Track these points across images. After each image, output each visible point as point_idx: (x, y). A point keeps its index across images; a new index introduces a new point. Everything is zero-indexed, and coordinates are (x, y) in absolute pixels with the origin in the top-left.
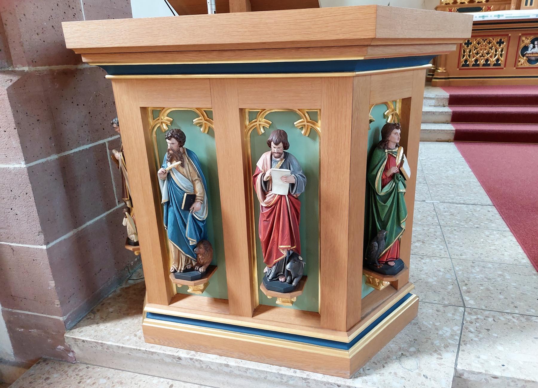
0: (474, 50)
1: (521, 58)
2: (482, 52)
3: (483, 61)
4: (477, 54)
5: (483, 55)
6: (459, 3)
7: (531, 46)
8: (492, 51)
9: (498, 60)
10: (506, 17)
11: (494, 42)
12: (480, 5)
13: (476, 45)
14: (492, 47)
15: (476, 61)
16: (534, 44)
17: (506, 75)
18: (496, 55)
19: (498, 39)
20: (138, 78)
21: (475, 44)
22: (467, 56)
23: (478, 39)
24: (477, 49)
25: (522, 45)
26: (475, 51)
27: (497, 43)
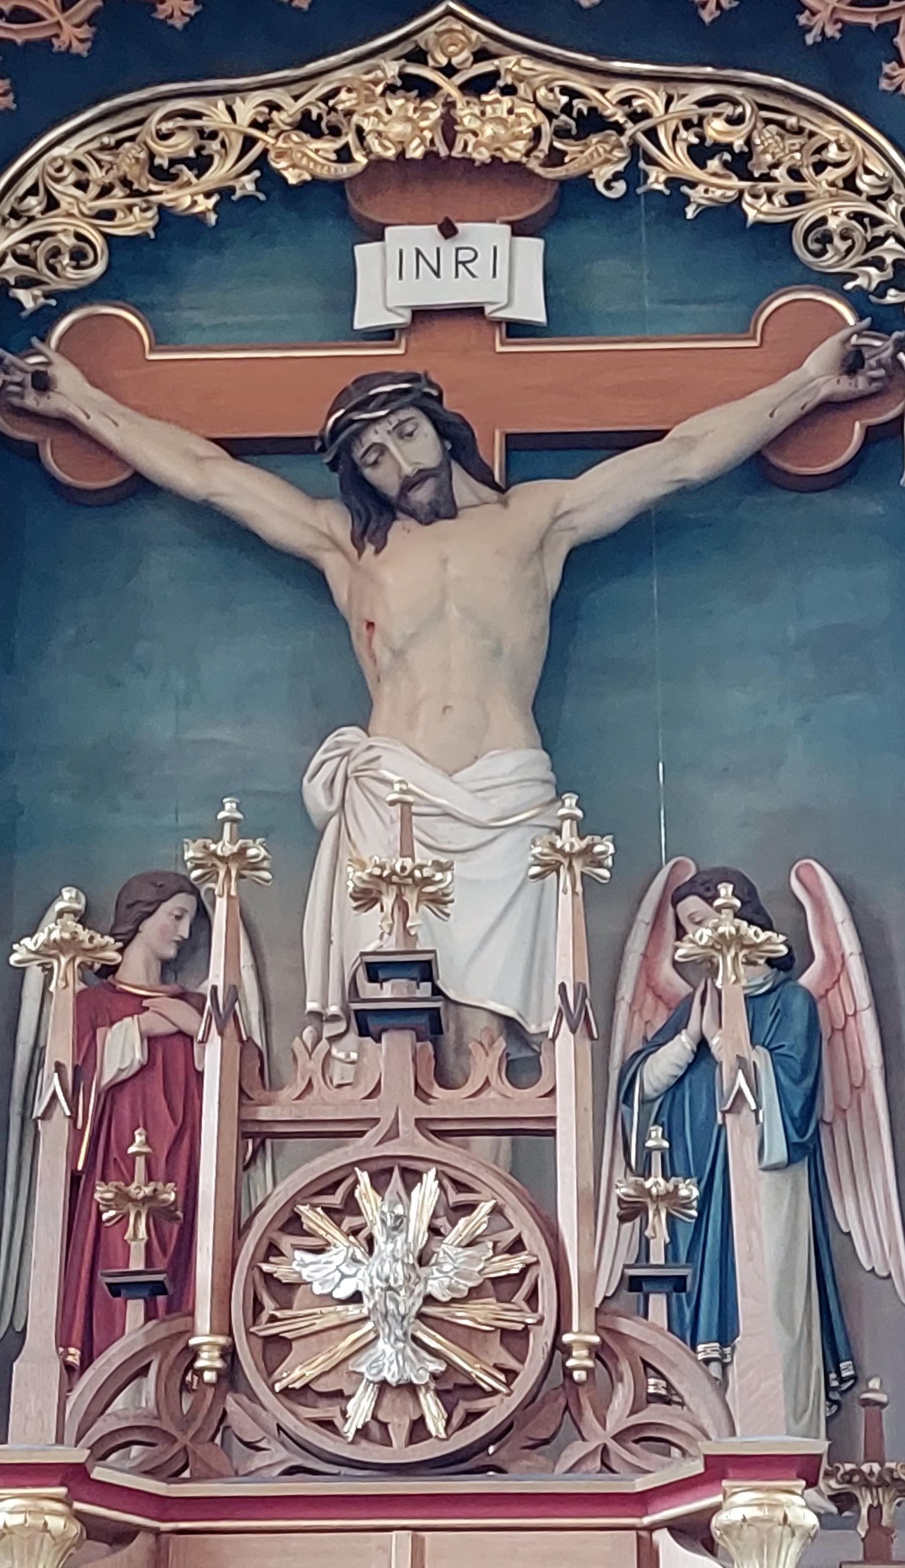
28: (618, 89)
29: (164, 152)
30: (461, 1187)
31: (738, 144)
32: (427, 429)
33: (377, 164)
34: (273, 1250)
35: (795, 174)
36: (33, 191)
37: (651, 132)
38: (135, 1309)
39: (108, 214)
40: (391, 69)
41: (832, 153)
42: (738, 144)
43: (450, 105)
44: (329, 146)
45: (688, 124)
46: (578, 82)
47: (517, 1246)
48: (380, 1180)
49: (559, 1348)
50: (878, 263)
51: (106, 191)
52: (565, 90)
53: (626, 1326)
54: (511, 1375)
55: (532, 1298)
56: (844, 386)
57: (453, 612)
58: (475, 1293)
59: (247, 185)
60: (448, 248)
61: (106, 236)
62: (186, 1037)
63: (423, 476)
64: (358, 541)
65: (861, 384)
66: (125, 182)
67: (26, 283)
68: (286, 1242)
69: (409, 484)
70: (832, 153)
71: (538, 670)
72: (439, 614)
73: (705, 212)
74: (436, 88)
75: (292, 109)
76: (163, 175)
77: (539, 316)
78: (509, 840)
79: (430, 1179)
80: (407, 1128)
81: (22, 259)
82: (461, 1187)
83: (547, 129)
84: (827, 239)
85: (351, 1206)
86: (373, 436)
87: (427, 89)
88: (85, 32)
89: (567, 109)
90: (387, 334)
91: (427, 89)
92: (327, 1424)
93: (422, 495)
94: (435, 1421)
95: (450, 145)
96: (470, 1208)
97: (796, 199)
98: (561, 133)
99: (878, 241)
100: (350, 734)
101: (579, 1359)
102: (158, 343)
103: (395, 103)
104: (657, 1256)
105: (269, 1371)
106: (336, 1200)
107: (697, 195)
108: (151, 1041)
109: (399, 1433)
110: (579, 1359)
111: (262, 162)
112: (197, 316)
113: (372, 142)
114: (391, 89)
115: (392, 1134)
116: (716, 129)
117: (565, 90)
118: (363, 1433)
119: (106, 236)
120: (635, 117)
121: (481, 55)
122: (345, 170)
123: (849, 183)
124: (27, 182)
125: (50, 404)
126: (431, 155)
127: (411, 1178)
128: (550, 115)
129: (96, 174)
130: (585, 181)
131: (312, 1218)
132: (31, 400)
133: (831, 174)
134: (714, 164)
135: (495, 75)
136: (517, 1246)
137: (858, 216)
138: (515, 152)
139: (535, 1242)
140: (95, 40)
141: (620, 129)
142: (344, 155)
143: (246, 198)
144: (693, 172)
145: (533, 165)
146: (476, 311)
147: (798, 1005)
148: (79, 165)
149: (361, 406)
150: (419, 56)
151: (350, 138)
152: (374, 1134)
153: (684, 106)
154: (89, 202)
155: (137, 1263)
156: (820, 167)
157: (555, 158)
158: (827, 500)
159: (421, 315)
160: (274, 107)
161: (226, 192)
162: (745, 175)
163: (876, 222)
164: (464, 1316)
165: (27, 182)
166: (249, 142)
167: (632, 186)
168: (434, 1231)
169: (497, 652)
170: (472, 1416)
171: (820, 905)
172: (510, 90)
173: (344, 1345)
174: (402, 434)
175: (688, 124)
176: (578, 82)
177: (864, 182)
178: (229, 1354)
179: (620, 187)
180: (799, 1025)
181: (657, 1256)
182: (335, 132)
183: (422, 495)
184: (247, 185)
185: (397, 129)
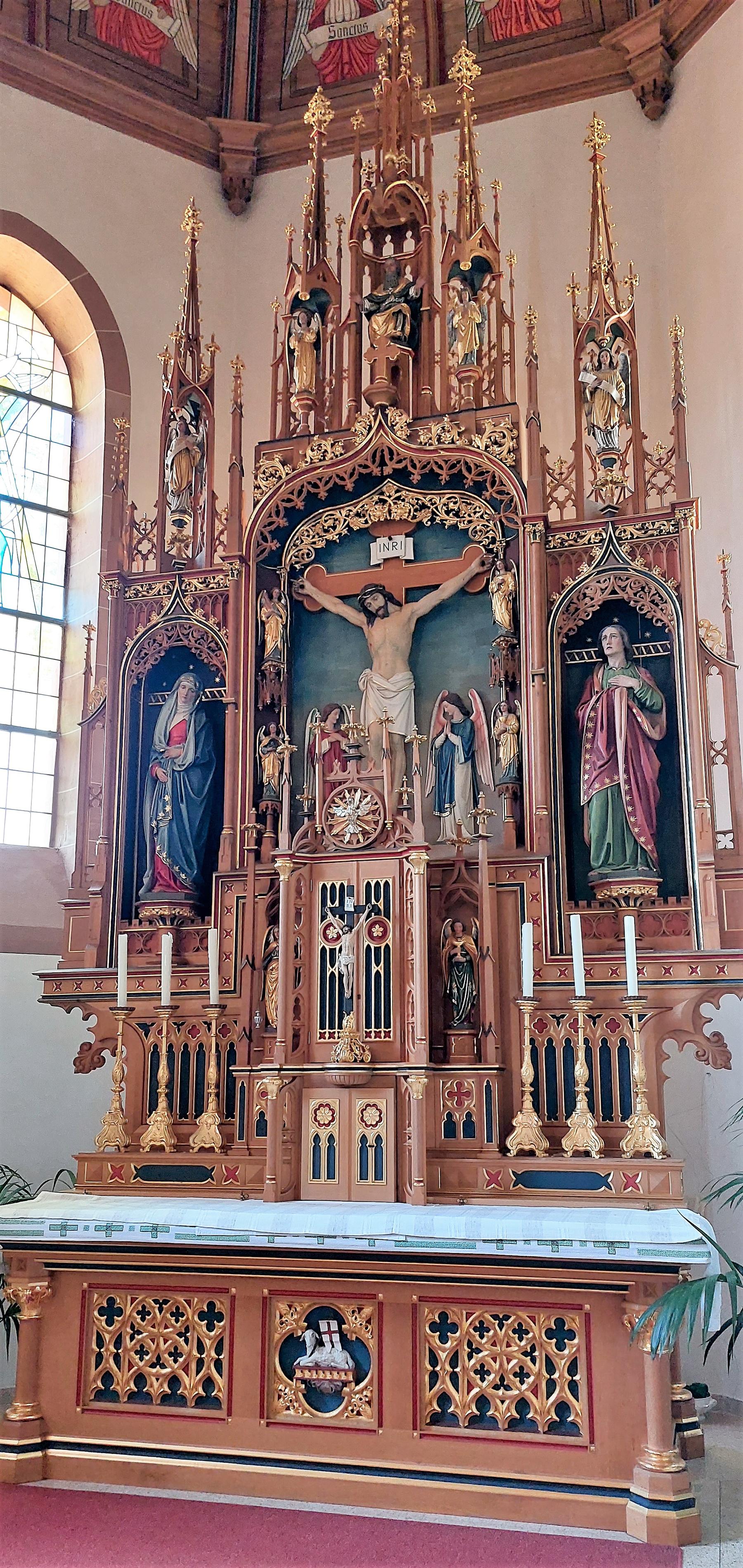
0: (470, 1357)
1: (281, 1381)
2: (496, 1366)
3: (508, 1409)
4: (482, 1372)
5: (502, 1379)
6: (513, 1152)
7: (309, 1336)
8: (535, 1369)
9: (562, 1408)
10: (178, 1236)
11: (537, 1331)
12: (205, 1161)
13: (135, 1319)
14: (533, 1349)
15: (482, 1402)
16: (317, 1329)
17: (385, 1459)
18: (551, 1385)
19: (549, 1318)
20: (259, 1471)
21: (468, 1333)
22: (562, 1390)
23: (140, 1298)
24: (478, 1351)
25: (278, 1336)
26: (473, 1361)
27: (550, 1333)
28: (428, 497)
29: (326, 525)
30: (365, 792)
31: (456, 508)
32: (381, 597)
33: (374, 523)
34: (330, 807)
35: (469, 515)
36: (297, 539)
37: (436, 508)
38: (306, 819)
39: (314, 543)
40: (376, 498)
41: (478, 509)
42: (456, 508)
43: (390, 505)
44: (362, 520)
45: (445, 505)
46: (420, 497)
47: (376, 804)
48: (349, 792)
49: (385, 824)
50: (488, 538)
51: (314, 537)
52: (416, 499)
53: (399, 818)
54: (375, 829)
55: (379, 814)
56: (481, 569)
57: (387, 641)
58: (368, 814)
59: (345, 532)
60: (391, 542)
61: (315, 549)
62: (339, 742)
63: (380, 608)
64: (368, 624)
65: (485, 568)
66: (318, 534)
67: (297, 563)
68: (332, 805)
69: (378, 610)
70: (478, 509)
71: (409, 650)
72: (384, 641)
73: (449, 527)
74: (386, 501)
75: (355, 511)
76: (326, 531)
77: (411, 557)
78: (401, 694)
79: (359, 791)
80: (356, 780)
81: (296, 557)
82: (365, 792)
83: (412, 510)
84: (476, 532)
85: (344, 797)
86: (368, 601)
87: (384, 502)
88: (303, 503)
89: (417, 503)
90: (378, 565)
91: (384, 502)
92: (342, 841)
93: (380, 613)
94: (361, 840)
95: (390, 516)
96: (366, 796)
97: (470, 522)
98: (416, 510)
99: (488, 532)
100: (368, 671)
101: (389, 826)
102: (328, 573)
103: (377, 507)
104: (405, 803)
105: (330, 831)
106: (341, 796)
107: (447, 523)
108: (331, 743)
109: (355, 842)
110: (389, 826)
111: (348, 525)
112: (338, 564)
113: (372, 518)
114: (376, 503)
115: (353, 781)
116: (451, 505)
117: (416, 499)
118: (348, 842)
119: (315, 549)
120: (432, 504)
121: (397, 492)
122: (366, 526)
123: (482, 517)
124: (296, 537)
125: (305, 592)
126: (386, 519)
127: (356, 791)
128: (413, 506)
129: (311, 533)
130: (421, 522)
131: (337, 800)
132: (300, 591)
133: (478, 515)
134: (451, 514)
135: (400, 496)
136: (376, 804)
137: (483, 525)
138: (405, 516)
139: (379, 803)
140: (305, 505)
141: (429, 508)
142: (366, 522)
143: (346, 535)
144: (446, 517)
145: (409, 519)
146: (398, 557)
147: (469, 725)
148: (307, 531)
149: (365, 595)
150: (382, 493)
151: (367, 517)
152: (349, 781)
153: (444, 500)
154: (310, 540)
155: (306, 810)
156: (475, 513)
157: (414, 517)
158: (480, 596)
159: (385, 560)
160: (350, 511)
161: (340, 534)
162: (458, 517)
163: (488, 526)
164: (366, 818)
165: (296, 537)
166: (345, 520)
167: (432, 523)
168: (360, 801)
169: (397, 650)
170: (368, 838)
171: (475, 699)
172: (403, 500)
173: (343, 825)
174: (375, 599)
175: (445, 505)
176: (420, 497)
177: (485, 516)
178: (322, 828)
179: (429, 523)
180: (468, 730)
181: (405, 803)
182: (364, 516)
183: (380, 613)
184: (345, 532)
185: (378, 513)
